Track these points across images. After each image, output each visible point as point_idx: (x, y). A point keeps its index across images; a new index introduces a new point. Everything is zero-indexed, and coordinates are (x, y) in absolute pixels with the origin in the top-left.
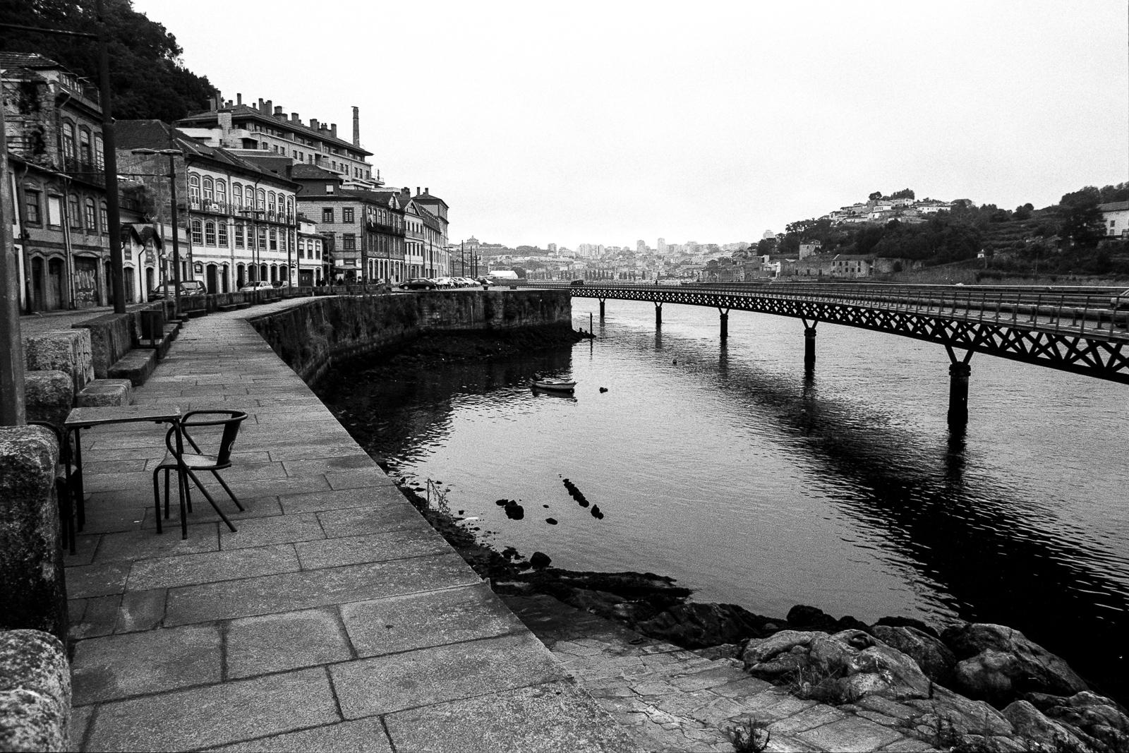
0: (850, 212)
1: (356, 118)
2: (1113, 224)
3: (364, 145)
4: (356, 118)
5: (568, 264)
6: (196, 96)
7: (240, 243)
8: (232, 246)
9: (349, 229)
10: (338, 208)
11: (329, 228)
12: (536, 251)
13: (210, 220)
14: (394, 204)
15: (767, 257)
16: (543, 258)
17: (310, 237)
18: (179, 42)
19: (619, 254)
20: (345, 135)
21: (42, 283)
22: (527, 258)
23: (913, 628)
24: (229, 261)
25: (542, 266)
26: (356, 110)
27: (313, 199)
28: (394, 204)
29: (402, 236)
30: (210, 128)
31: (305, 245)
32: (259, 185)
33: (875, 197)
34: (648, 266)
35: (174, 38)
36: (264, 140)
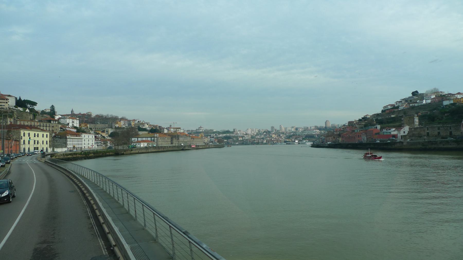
5: (242, 137)
12: (228, 132)
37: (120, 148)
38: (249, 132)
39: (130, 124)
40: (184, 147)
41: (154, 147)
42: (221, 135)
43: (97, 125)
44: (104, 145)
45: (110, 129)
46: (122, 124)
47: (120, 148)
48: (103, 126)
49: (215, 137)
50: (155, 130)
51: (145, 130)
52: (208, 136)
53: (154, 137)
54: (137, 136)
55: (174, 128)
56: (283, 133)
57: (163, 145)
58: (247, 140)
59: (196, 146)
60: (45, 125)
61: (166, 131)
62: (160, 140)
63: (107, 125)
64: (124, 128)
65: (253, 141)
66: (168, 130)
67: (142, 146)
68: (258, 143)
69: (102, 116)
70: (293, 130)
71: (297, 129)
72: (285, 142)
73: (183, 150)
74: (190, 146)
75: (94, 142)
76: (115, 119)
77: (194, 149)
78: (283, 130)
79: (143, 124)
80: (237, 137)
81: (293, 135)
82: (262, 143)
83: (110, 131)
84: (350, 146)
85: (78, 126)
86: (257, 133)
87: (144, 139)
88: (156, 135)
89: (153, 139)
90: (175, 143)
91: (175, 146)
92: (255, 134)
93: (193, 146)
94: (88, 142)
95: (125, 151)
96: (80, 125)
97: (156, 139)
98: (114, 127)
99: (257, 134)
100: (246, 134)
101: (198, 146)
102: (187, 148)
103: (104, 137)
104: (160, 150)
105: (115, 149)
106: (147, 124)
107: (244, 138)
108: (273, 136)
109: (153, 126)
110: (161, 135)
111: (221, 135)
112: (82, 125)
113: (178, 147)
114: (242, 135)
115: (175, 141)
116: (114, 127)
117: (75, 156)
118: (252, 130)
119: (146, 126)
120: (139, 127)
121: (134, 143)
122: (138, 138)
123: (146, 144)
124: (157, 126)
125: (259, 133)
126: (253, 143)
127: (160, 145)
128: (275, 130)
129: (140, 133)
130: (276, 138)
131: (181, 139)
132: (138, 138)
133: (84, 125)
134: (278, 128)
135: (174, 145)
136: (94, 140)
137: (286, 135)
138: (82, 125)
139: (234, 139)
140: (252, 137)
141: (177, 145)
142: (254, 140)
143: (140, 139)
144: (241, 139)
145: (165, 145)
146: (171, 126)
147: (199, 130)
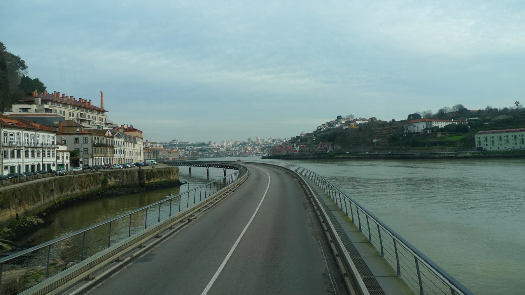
0: (329, 124)
1: (102, 96)
2: (418, 127)
3: (105, 109)
4: (102, 96)
5: (217, 149)
6: (32, 89)
7: (27, 156)
9: (86, 146)
10: (81, 138)
11: (78, 146)
12: (203, 144)
13: (12, 149)
14: (109, 134)
15: (295, 144)
16: (207, 147)
17: (63, 151)
18: (26, 64)
20: (96, 103)
21: (295, 161)
22: (199, 147)
24: (21, 164)
26: (102, 93)
27: (70, 134)
28: (109, 134)
29: (113, 147)
30: (30, 104)
31: (60, 155)
32: (37, 133)
33: (339, 118)
35: (24, 62)
36: (55, 108)
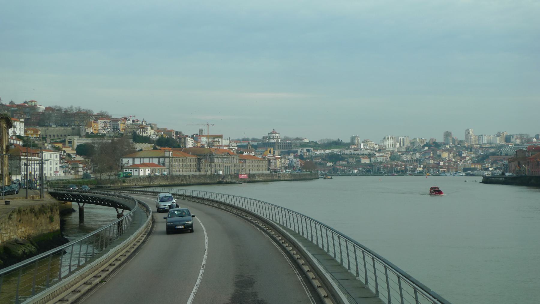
5: (370, 156)
8: (9, 199)
12: (337, 144)
19: (423, 147)
23: (181, 227)
25: (343, 159)
34: (454, 157)
37: (105, 176)
38: (388, 145)
39: (116, 128)
40: (224, 177)
41: (163, 176)
42: (319, 152)
43: (51, 129)
44: (72, 172)
45: (76, 138)
46: (100, 127)
47: (105, 176)
48: (59, 130)
49: (306, 155)
50: (169, 142)
51: (147, 140)
52: (289, 153)
53: (164, 157)
54: (132, 153)
55: (208, 137)
56: (470, 149)
57: (181, 173)
58: (381, 163)
59: (249, 175)
60: (184, 170)
61: (190, 144)
62: (175, 163)
63: (69, 129)
64: (103, 136)
65: (393, 167)
66: (196, 141)
67: (142, 173)
68: (403, 173)
69: (59, 110)
70: (498, 141)
71: (508, 139)
72: (465, 170)
73: (220, 183)
74: (236, 175)
75: (59, 165)
76: (83, 117)
77: (243, 181)
78: (474, 140)
79: (143, 127)
80: (358, 157)
81: (493, 154)
82: (413, 172)
83: (77, 141)
84: (533, 181)
85: (22, 134)
86: (408, 148)
87: (146, 161)
88: (167, 154)
89: (162, 160)
90: (206, 170)
91: (204, 176)
92: (404, 149)
93: (243, 176)
94: (52, 166)
95: (113, 182)
96: (25, 132)
97: (167, 160)
98: (83, 134)
99: (407, 151)
100: (380, 151)
101: (254, 175)
102: (228, 180)
103: (69, 155)
104: (175, 183)
105: (96, 179)
106: (152, 128)
107: (373, 159)
108: (445, 155)
109: (165, 131)
110: (178, 153)
111: (319, 152)
112: (29, 132)
113: (210, 177)
114: (369, 152)
115: (204, 164)
116: (83, 134)
117: (337, 151)
118: (396, 140)
119: (150, 133)
120: (135, 133)
121: (128, 167)
122: (134, 158)
123: (148, 171)
124: (171, 131)
125: (412, 148)
126: (391, 172)
127: (175, 173)
128: (454, 141)
129: (138, 146)
130: (449, 161)
131: (218, 161)
132: (134, 158)
133: (32, 132)
134: (460, 137)
135: (203, 173)
136: (58, 162)
137: (476, 152)
138: (29, 132)
139: (351, 161)
140: (393, 157)
141: (209, 173)
142: (397, 166)
143: (137, 161)
144: (367, 161)
145: (184, 174)
146: (201, 131)
147: (269, 138)
